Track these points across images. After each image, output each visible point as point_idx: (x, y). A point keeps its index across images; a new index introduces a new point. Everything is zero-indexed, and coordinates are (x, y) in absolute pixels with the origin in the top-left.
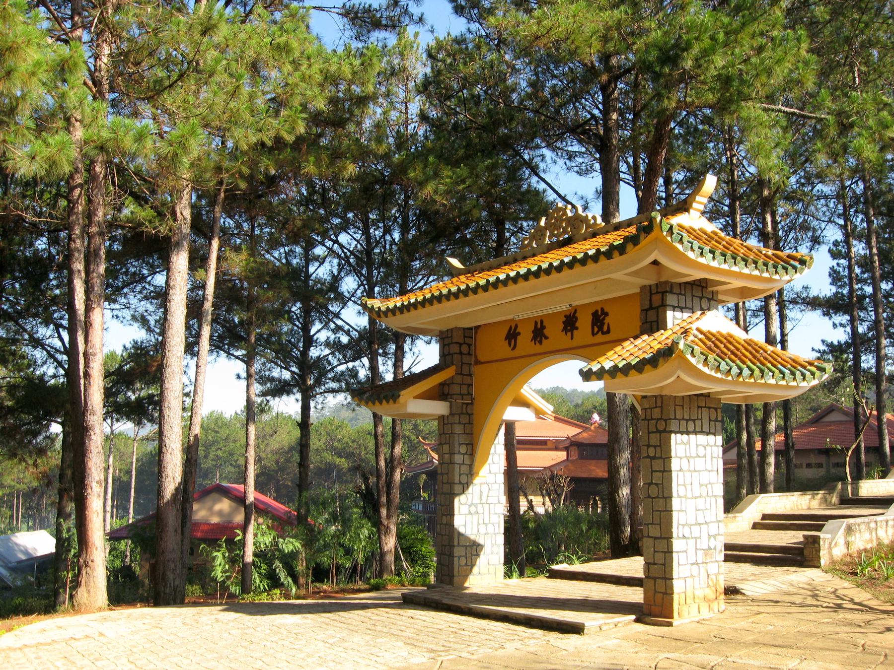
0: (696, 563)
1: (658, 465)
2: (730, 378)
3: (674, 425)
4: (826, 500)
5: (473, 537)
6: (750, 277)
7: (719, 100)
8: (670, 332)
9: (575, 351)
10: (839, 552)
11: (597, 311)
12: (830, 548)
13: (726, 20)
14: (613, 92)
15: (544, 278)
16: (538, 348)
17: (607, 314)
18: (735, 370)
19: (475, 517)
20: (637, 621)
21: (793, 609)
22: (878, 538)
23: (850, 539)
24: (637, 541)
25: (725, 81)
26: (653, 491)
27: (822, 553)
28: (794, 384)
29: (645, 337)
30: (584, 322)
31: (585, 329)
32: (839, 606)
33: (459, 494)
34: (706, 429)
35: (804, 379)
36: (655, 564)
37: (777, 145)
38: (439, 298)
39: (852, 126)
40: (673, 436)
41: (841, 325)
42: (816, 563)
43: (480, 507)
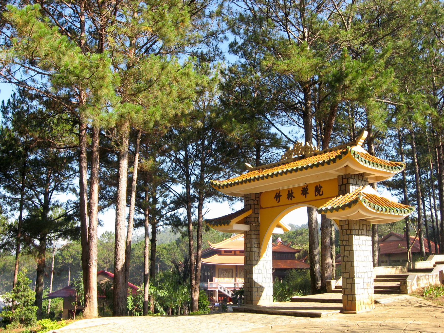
0: (363, 289)
1: (347, 248)
2: (378, 212)
3: (354, 232)
4: (402, 270)
5: (260, 284)
6: (382, 172)
7: (359, 97)
8: (351, 194)
10: (415, 288)
11: (317, 186)
12: (411, 286)
13: (361, 64)
14: (309, 92)
15: (299, 172)
16: (290, 202)
17: (321, 187)
18: (380, 209)
19: (261, 274)
20: (341, 312)
21: (402, 307)
22: (429, 283)
23: (419, 282)
24: (325, 287)
25: (362, 90)
26: (346, 259)
27: (408, 288)
28: (401, 215)
29: (341, 196)
30: (311, 191)
31: (311, 194)
32: (421, 306)
33: (255, 265)
34: (365, 234)
35: (405, 213)
36: (347, 289)
37: (382, 116)
38: (250, 180)
39: (412, 108)
40: (354, 236)
41: (395, 195)
42: (406, 292)
43: (263, 270)
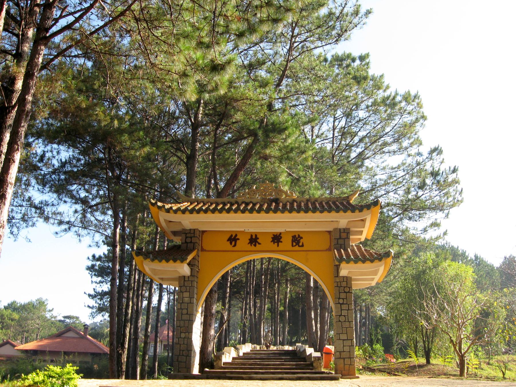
9: (279, 252)
11: (295, 236)
16: (253, 248)
17: (302, 238)
36: (344, 352)
